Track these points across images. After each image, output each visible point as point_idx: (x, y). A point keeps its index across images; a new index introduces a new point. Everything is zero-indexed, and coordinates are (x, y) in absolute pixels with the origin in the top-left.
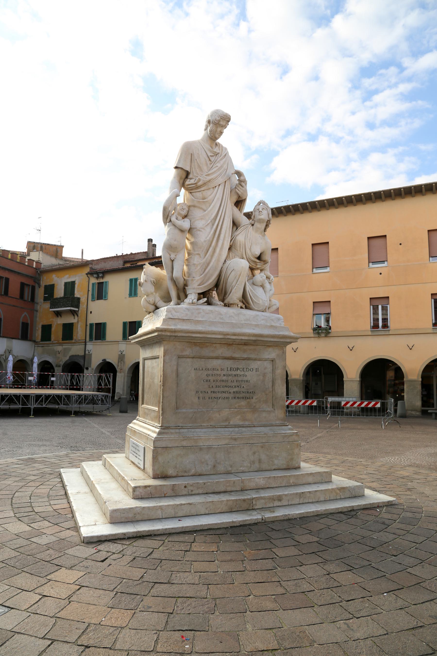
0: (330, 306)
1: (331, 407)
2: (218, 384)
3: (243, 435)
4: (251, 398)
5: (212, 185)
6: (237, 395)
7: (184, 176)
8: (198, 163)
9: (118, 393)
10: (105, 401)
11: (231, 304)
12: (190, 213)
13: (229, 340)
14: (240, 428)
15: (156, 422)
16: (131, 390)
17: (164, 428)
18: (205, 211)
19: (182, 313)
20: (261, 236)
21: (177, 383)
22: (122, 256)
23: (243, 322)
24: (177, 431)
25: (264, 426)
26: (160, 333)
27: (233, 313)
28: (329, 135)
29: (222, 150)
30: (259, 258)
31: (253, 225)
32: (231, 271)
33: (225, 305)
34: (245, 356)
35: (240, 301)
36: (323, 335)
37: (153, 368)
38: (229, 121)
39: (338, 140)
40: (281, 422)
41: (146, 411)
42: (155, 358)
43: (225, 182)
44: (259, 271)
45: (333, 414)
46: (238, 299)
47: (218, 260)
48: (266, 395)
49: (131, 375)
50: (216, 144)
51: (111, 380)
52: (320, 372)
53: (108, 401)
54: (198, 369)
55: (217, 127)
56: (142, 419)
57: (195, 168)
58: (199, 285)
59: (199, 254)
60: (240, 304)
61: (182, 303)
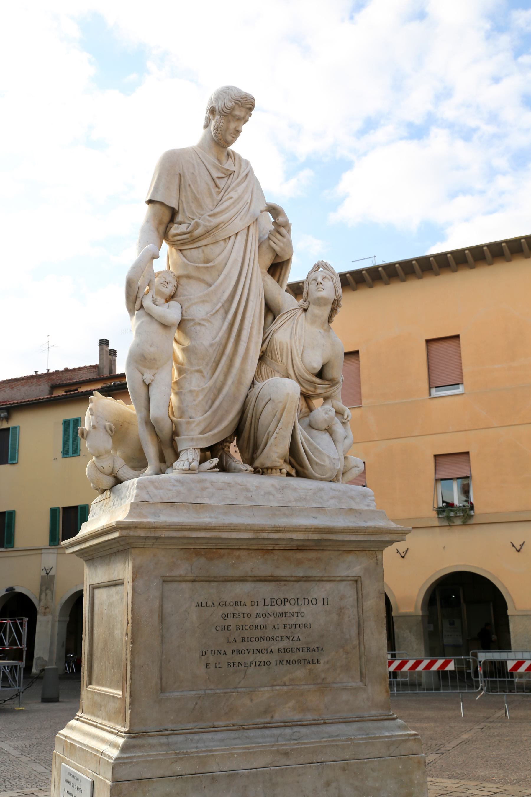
0: (469, 461)
1: (485, 673)
2: (247, 634)
3: (305, 743)
4: (316, 661)
5: (222, 234)
6: (287, 656)
7: (166, 218)
8: (192, 192)
9: (39, 658)
10: (10, 679)
11: (268, 468)
12: (180, 290)
13: (266, 542)
14: (296, 729)
15: (117, 723)
16: (68, 652)
17: (136, 736)
18: (210, 286)
19: (170, 490)
20: (322, 331)
21: (162, 636)
22: (48, 375)
23: (294, 504)
24: (164, 740)
25: (347, 721)
26: (125, 533)
27: (273, 485)
28: (451, 126)
29: (240, 165)
30: (320, 374)
31: (305, 310)
32: (264, 403)
33: (256, 471)
34: (300, 573)
35: (285, 461)
36: (458, 522)
37: (112, 605)
38: (251, 109)
39: (467, 135)
40: (381, 712)
41: (97, 698)
42: (115, 585)
43: (249, 227)
44: (321, 400)
45: (492, 688)
46: (282, 458)
47: (239, 381)
48: (347, 653)
49: (68, 619)
50: (228, 155)
51: (24, 632)
52: (458, 597)
53: (17, 677)
54: (204, 604)
55: (229, 122)
56: (88, 717)
57: (188, 203)
58: (202, 433)
59: (200, 371)
60: (286, 468)
61: (169, 470)
